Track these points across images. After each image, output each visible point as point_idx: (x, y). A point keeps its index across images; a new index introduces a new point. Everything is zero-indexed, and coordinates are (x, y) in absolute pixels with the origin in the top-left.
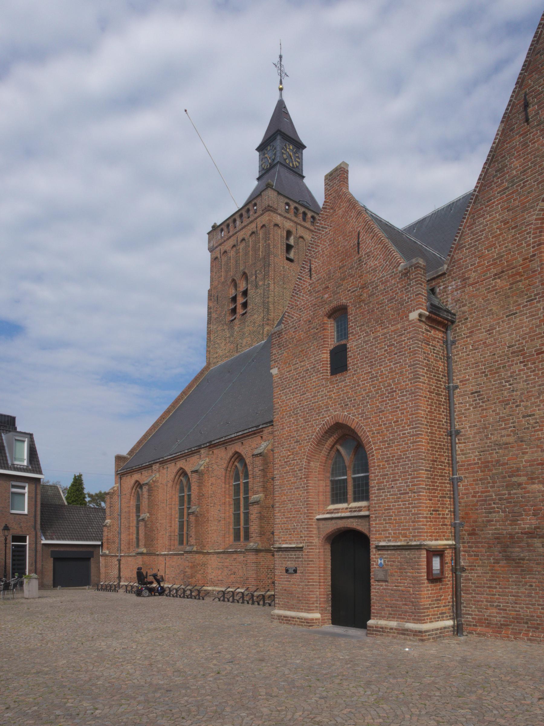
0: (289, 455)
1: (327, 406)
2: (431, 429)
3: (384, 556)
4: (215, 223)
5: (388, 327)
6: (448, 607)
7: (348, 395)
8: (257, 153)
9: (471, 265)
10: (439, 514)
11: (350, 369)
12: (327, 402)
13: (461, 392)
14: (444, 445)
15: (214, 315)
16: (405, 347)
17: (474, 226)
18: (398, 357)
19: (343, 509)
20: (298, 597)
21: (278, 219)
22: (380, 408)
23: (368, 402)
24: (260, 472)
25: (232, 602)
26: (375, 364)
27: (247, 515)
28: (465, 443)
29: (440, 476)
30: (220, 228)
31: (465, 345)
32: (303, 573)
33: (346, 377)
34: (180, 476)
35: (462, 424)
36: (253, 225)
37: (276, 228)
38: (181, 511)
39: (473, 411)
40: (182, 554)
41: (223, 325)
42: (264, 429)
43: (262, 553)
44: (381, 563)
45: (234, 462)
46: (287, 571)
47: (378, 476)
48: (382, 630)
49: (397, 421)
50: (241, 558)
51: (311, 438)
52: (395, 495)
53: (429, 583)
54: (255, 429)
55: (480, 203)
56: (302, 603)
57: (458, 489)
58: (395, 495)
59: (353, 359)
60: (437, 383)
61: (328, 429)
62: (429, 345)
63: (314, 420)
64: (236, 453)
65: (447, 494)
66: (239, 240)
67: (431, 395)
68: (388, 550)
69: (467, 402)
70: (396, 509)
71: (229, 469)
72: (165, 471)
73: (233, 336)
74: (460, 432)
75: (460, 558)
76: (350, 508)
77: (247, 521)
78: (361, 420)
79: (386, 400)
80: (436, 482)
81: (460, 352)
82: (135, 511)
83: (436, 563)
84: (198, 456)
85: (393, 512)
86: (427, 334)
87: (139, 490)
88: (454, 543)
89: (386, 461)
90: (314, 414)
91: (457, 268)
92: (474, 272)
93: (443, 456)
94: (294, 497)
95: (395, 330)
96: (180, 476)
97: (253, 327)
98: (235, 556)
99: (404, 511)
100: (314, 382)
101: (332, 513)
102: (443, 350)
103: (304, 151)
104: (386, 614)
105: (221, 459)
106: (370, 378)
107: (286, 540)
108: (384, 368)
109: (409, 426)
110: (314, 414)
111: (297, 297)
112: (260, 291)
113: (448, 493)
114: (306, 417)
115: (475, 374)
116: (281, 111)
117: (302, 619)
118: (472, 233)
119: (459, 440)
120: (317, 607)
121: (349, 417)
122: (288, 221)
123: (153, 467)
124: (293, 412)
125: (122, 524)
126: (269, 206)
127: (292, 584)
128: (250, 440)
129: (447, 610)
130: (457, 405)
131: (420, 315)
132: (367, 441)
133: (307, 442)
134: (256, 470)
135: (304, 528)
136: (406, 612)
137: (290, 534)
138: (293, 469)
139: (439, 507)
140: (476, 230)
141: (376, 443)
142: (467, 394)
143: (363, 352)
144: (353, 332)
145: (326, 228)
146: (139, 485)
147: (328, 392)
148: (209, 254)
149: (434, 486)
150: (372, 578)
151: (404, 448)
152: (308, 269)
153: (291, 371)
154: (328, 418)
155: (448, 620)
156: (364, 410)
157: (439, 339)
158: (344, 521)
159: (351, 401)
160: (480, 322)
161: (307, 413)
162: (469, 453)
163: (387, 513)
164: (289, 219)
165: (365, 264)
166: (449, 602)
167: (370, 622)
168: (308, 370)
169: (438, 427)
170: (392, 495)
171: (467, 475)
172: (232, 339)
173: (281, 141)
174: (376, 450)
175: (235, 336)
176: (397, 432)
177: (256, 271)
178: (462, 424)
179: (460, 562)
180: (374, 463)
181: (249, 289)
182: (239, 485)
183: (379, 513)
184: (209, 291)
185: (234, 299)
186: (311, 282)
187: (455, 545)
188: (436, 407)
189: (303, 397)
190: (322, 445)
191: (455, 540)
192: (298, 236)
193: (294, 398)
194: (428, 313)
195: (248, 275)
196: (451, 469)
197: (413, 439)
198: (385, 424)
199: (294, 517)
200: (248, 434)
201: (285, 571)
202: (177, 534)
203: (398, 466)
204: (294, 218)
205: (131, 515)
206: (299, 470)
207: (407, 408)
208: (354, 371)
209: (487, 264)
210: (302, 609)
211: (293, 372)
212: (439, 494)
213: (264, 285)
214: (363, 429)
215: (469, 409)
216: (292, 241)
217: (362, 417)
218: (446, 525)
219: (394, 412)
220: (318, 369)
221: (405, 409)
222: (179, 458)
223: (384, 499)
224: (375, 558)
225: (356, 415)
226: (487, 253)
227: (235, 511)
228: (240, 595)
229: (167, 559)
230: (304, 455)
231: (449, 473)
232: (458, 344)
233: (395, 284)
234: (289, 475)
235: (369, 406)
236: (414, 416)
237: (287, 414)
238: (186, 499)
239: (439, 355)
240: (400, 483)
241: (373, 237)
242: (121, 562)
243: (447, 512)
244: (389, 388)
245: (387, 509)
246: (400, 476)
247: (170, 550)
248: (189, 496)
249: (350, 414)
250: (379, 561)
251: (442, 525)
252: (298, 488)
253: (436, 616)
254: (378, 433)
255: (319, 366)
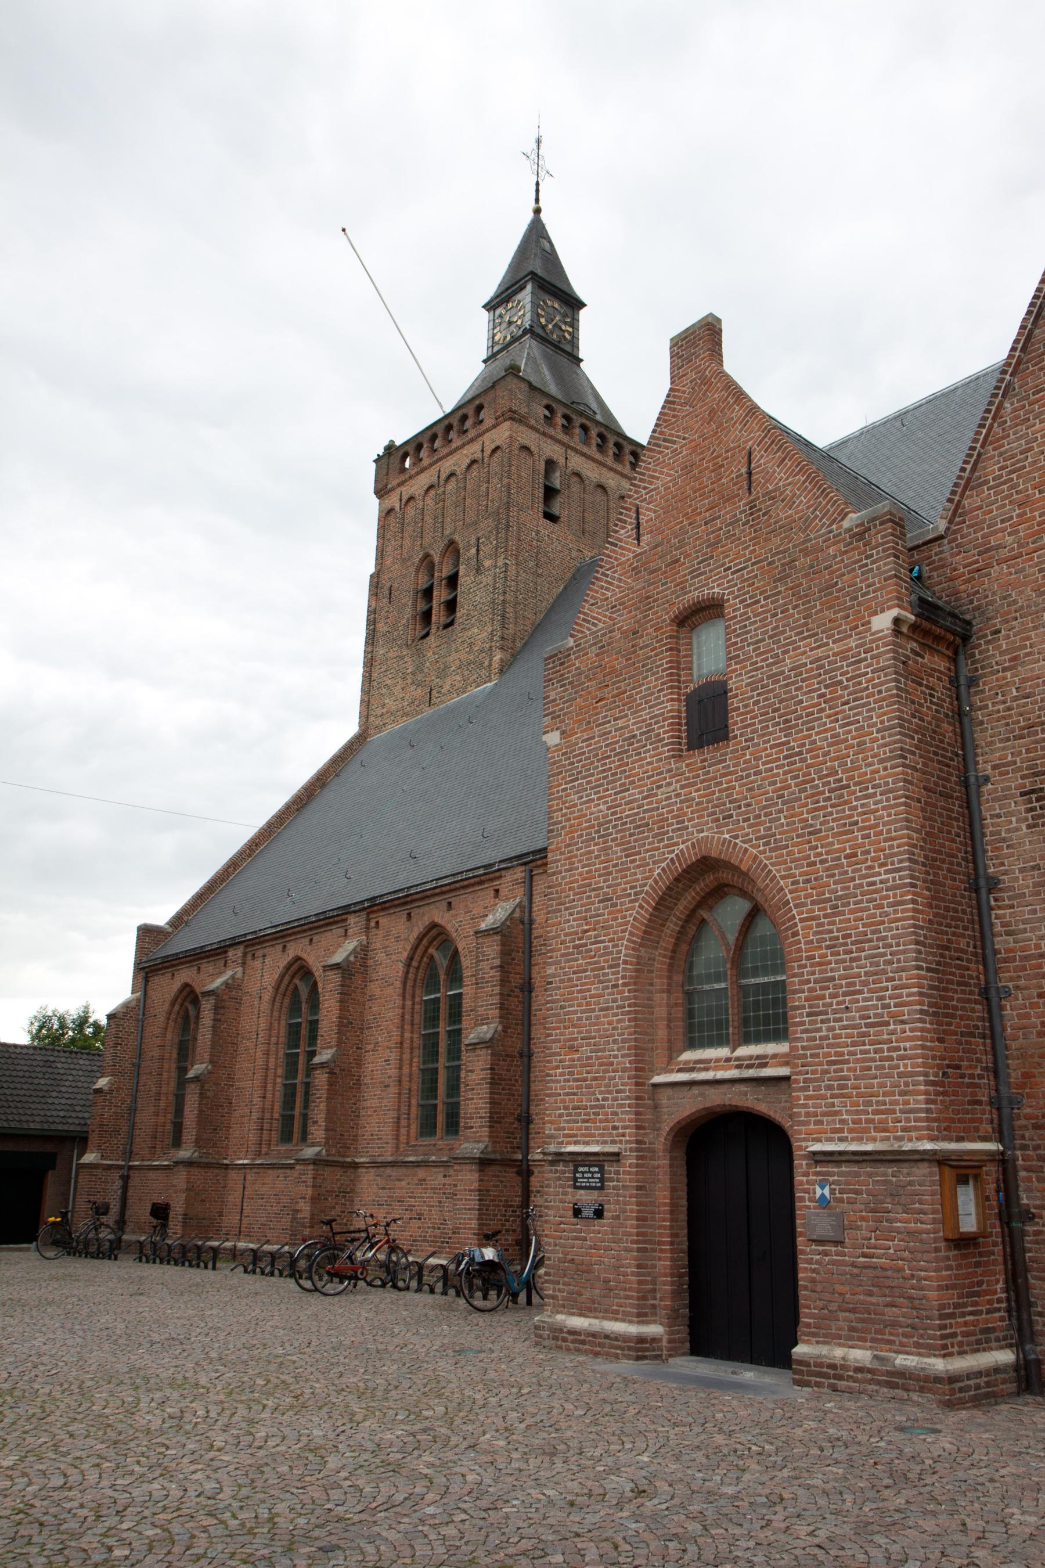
0: (586, 931)
1: (680, 817)
2: (935, 875)
3: (831, 1179)
4: (392, 442)
5: (827, 644)
6: (997, 1315)
7: (732, 795)
8: (485, 315)
9: (1003, 521)
10: (963, 1076)
11: (735, 737)
12: (680, 809)
13: (996, 790)
14: (964, 912)
15: (382, 627)
16: (867, 688)
17: (1005, 441)
18: (850, 709)
19: (718, 1060)
20: (607, 1281)
21: (527, 437)
22: (811, 826)
23: (781, 811)
24: (492, 973)
25: (416, 1291)
26: (797, 725)
27: (454, 1073)
28: (1012, 907)
29: (959, 984)
30: (401, 453)
31: (1000, 687)
32: (618, 1217)
33: (726, 754)
34: (293, 977)
35: (1003, 864)
36: (476, 447)
37: (524, 454)
38: (292, 1061)
39: (1026, 834)
40: (291, 1167)
41: (400, 647)
42: (503, 873)
43: (492, 1168)
44: (823, 1195)
45: (427, 948)
46: (577, 1212)
47: (808, 981)
48: (830, 1376)
49: (855, 855)
50: (436, 1178)
51: (642, 892)
52: (854, 1027)
53: (948, 1249)
54: (481, 871)
55: (1015, 395)
56: (617, 1296)
57: (1002, 1016)
58: (854, 1027)
59: (742, 714)
60: (941, 770)
61: (684, 871)
62: (921, 685)
63: (648, 851)
64: (434, 925)
65: (977, 1027)
66: (443, 476)
67: (931, 797)
68: (838, 1163)
69: (1010, 814)
70: (856, 1061)
71: (415, 963)
72: (258, 963)
73: (422, 671)
74: (999, 882)
75: (1017, 1186)
76: (738, 1059)
77: (454, 1087)
78: (764, 852)
79: (825, 807)
80: (952, 999)
81: (990, 703)
82: (175, 1056)
83: (967, 1199)
84: (341, 931)
85: (849, 1069)
86: (916, 662)
87: (190, 1007)
88: (1001, 1148)
89: (828, 947)
90: (648, 837)
91: (968, 527)
92: (1010, 534)
93: (963, 936)
94: (599, 1030)
95: (842, 652)
96: (293, 977)
97: (469, 653)
98: (421, 1173)
99: (877, 1068)
100: (648, 764)
101: (691, 1070)
102: (950, 697)
103: (583, 313)
104: (840, 1329)
105: (398, 939)
106: (786, 757)
107: (576, 1136)
108: (817, 734)
109: (881, 865)
110: (648, 837)
111: (606, 582)
112: (486, 579)
113: (980, 1024)
114: (629, 842)
115: (1028, 751)
116: (537, 233)
117: (616, 1339)
118: (1000, 455)
119: (996, 900)
120: (654, 1306)
121: (736, 844)
122: (549, 441)
123: (230, 953)
124: (598, 832)
125: (141, 1088)
126: (510, 410)
127: (591, 1247)
128: (470, 897)
129: (998, 1320)
130: (989, 821)
131: (897, 621)
132: (780, 900)
133: (630, 902)
134: (485, 965)
135: (621, 1106)
136: (895, 1324)
137: (587, 1121)
138: (595, 963)
139: (961, 1059)
140: (1011, 449)
141: (804, 905)
142: (1012, 796)
143: (766, 699)
144: (738, 656)
145: (674, 442)
146: (189, 996)
147: (682, 787)
148: (375, 501)
149: (946, 1007)
150: (802, 1234)
151: (874, 916)
152: (631, 524)
153: (593, 738)
154: (681, 846)
155: (1002, 1348)
156: (770, 828)
157: (941, 672)
158: (723, 1089)
159: (740, 807)
160: (1029, 638)
161: (631, 835)
162: (1025, 931)
163: (835, 1071)
164: (552, 438)
165: (764, 515)
166: (999, 1301)
167: (800, 1350)
168: (634, 736)
169: (949, 871)
170: (845, 1028)
171: (1022, 983)
172: (420, 677)
173: (539, 288)
174: (801, 920)
175: (426, 670)
176: (853, 879)
177: (478, 539)
178: (1003, 864)
179: (1018, 1198)
180: (800, 950)
181: (461, 573)
182: (437, 1001)
183: (814, 1072)
184: (371, 576)
185: (428, 593)
186: (639, 551)
187: (1003, 1153)
188: (942, 823)
189: (621, 799)
190: (668, 908)
191: (1001, 1141)
192: (569, 471)
193: (599, 799)
194: (913, 617)
195: (461, 546)
196: (981, 967)
197: (895, 896)
198: (822, 862)
199: (595, 1079)
200: (466, 883)
201: (571, 1213)
202: (276, 1116)
203: (859, 959)
204: (561, 436)
205: (166, 1066)
206: (611, 967)
207: (877, 825)
208: (746, 741)
209: (1038, 519)
210: (617, 1312)
211: (599, 742)
212: (958, 1026)
213: (496, 567)
214: (770, 871)
215: (1017, 829)
216: (557, 482)
217: (765, 844)
218: (979, 1102)
219: (845, 833)
220: (659, 734)
221: (870, 827)
222: (295, 933)
223: (827, 1038)
224: (808, 1183)
225: (751, 840)
226: (1037, 495)
227: (424, 1063)
228: (440, 1273)
229: (249, 1177)
230: (623, 931)
231: (978, 978)
232: (984, 685)
233: (835, 556)
234: (586, 977)
235: (783, 821)
236: (895, 843)
237: (581, 836)
238: (304, 1032)
239: (942, 707)
240: (865, 1000)
241: (783, 460)
242: (131, 1183)
243: (979, 1072)
244: (831, 779)
245: (834, 1063)
246: (865, 983)
247: (258, 1154)
248: (314, 1025)
249: (736, 837)
250: (819, 1192)
251: (970, 1103)
252: (607, 1009)
253: (973, 1338)
254: (808, 881)
255: (659, 728)
